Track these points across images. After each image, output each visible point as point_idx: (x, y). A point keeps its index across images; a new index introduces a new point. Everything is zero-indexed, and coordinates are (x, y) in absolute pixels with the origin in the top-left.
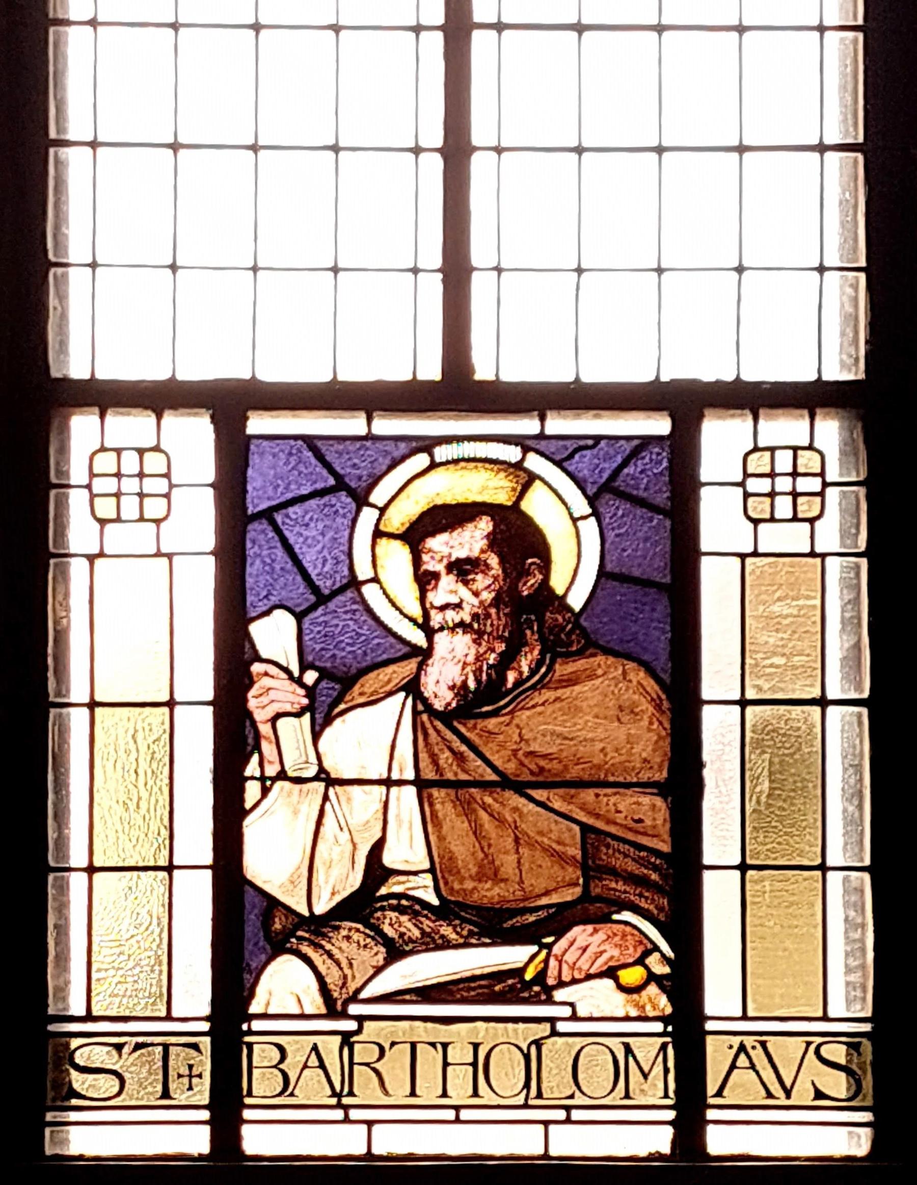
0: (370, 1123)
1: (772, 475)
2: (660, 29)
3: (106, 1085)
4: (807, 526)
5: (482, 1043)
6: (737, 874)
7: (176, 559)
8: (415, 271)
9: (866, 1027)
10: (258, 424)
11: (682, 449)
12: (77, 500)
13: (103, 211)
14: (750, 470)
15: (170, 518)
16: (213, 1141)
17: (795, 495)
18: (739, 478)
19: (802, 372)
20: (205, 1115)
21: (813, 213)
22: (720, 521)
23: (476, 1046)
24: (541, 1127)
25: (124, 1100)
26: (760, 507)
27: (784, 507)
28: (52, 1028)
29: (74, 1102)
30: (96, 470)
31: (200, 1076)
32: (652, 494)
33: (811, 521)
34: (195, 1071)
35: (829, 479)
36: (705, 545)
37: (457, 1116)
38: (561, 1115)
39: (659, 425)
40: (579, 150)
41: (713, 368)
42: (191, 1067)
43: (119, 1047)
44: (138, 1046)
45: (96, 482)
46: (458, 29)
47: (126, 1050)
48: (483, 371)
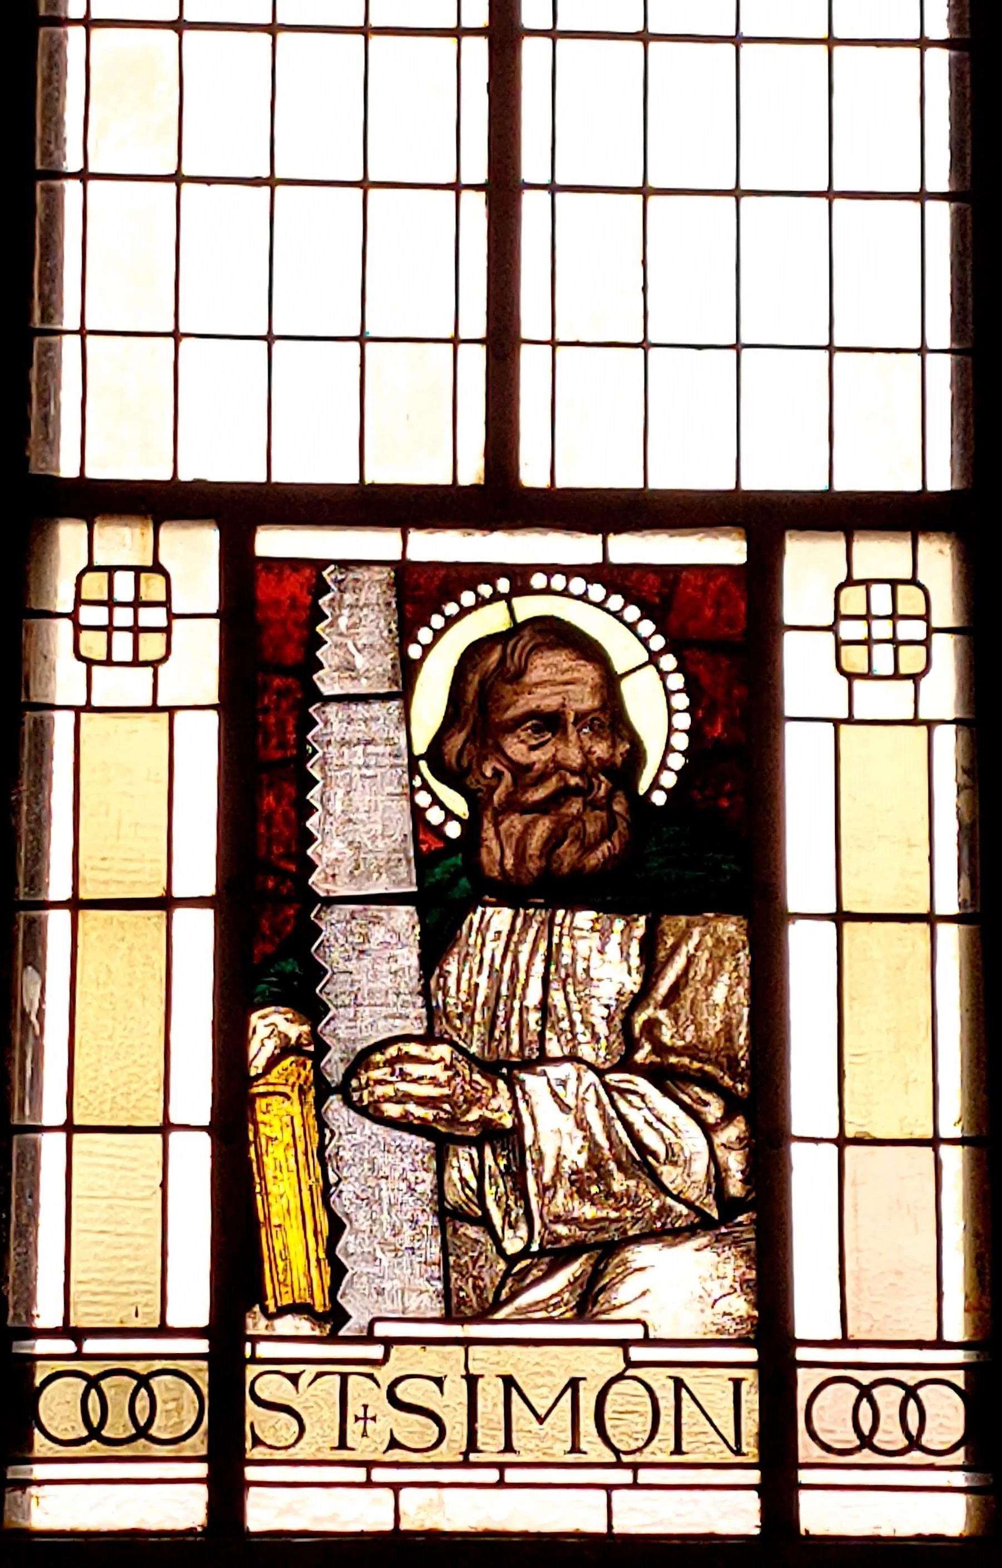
0: (396, 1487)
1: (868, 617)
2: (271, 182)
3: (284, 1427)
5: (482, 1376)
6: (834, 1149)
7: (179, 716)
8: (554, 343)
10: (273, 542)
11: (762, 575)
12: (946, 611)
13: (109, 256)
15: (171, 658)
16: (211, 1506)
17: (895, 642)
20: (805, 1476)
21: (903, 273)
24: (388, 1494)
26: (855, 658)
27: (123, 646)
30: (844, 610)
31: (357, 1419)
32: (726, 640)
35: (935, 623)
36: (791, 707)
39: (728, 550)
43: (294, 1379)
44: (319, 1375)
45: (84, 610)
46: (504, 34)
47: (304, 1381)
48: (532, 474)
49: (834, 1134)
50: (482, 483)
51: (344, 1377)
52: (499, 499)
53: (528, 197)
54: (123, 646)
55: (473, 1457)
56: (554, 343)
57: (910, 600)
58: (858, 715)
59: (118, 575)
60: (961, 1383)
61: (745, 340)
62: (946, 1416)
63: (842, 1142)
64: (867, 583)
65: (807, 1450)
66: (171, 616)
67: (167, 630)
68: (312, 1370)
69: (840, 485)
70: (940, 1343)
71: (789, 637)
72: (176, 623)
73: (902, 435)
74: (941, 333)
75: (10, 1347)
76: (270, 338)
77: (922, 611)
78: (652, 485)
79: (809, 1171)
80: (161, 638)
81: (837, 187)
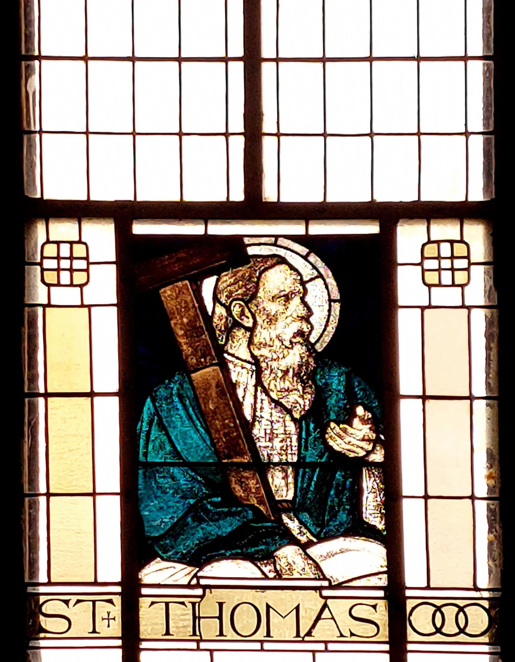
0: (211, 651)
2: (370, 59)
3: (60, 625)
4: (78, 289)
5: (225, 602)
6: (423, 500)
7: (93, 309)
9: (118, 589)
10: (140, 228)
11: (386, 242)
14: (426, 255)
15: (90, 283)
18: (419, 261)
19: (455, 195)
20: (387, 647)
21: (460, 97)
22: (408, 287)
23: (221, 605)
25: (256, 637)
26: (432, 278)
28: (30, 590)
29: (42, 635)
33: (81, 286)
34: (111, 617)
37: (326, 647)
38: (322, 646)
39: (372, 228)
40: (133, 59)
41: (407, 195)
42: (109, 614)
43: (67, 602)
44: (78, 601)
45: (45, 261)
47: (71, 603)
48: (269, 194)
49: (422, 494)
50: (264, 200)
51: (167, 604)
52: (254, 206)
53: (265, 66)
54: (65, 278)
55: (307, 639)
56: (467, 134)
57: (460, 250)
58: (433, 304)
59: (442, 245)
60: (487, 607)
61: (375, 131)
62: (479, 620)
63: (426, 497)
64: (438, 242)
65: (411, 636)
66: (89, 264)
67: (87, 270)
68: (74, 599)
69: (140, 198)
70: (476, 589)
71: (400, 268)
72: (91, 266)
73: (458, 172)
74: (477, 123)
75: (26, 589)
76: (325, 135)
77: (85, 255)
78: (186, 199)
79: (411, 512)
80: (85, 274)
81: (374, 55)
